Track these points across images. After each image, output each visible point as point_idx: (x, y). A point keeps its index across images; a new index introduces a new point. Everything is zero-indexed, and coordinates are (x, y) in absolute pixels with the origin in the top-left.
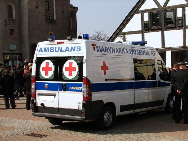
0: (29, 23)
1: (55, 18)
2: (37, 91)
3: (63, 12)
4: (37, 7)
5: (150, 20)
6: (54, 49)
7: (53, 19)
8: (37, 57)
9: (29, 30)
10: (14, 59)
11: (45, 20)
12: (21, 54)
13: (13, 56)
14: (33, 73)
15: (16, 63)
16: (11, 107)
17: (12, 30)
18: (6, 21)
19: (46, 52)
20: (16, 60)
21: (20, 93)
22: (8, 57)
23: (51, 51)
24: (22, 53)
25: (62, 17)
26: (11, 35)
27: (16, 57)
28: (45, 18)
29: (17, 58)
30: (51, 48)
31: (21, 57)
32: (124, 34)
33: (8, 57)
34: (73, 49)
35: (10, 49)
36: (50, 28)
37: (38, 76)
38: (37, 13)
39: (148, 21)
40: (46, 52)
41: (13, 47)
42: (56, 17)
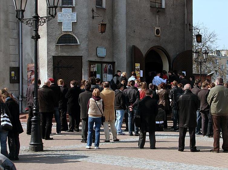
0: (127, 14)
7: (160, 7)
10: (103, 72)
11: (150, 8)
12: (113, 63)
15: (106, 76)
16: (147, 145)
17: (104, 25)
18: (93, 11)
20: (106, 72)
21: (67, 123)
22: (95, 69)
24: (115, 61)
25: (174, 4)
26: (102, 32)
27: (106, 67)
28: (149, 6)
29: (107, 69)
33: (95, 67)
35: (98, 55)
36: (156, 21)
41: (102, 52)
42: (166, 4)
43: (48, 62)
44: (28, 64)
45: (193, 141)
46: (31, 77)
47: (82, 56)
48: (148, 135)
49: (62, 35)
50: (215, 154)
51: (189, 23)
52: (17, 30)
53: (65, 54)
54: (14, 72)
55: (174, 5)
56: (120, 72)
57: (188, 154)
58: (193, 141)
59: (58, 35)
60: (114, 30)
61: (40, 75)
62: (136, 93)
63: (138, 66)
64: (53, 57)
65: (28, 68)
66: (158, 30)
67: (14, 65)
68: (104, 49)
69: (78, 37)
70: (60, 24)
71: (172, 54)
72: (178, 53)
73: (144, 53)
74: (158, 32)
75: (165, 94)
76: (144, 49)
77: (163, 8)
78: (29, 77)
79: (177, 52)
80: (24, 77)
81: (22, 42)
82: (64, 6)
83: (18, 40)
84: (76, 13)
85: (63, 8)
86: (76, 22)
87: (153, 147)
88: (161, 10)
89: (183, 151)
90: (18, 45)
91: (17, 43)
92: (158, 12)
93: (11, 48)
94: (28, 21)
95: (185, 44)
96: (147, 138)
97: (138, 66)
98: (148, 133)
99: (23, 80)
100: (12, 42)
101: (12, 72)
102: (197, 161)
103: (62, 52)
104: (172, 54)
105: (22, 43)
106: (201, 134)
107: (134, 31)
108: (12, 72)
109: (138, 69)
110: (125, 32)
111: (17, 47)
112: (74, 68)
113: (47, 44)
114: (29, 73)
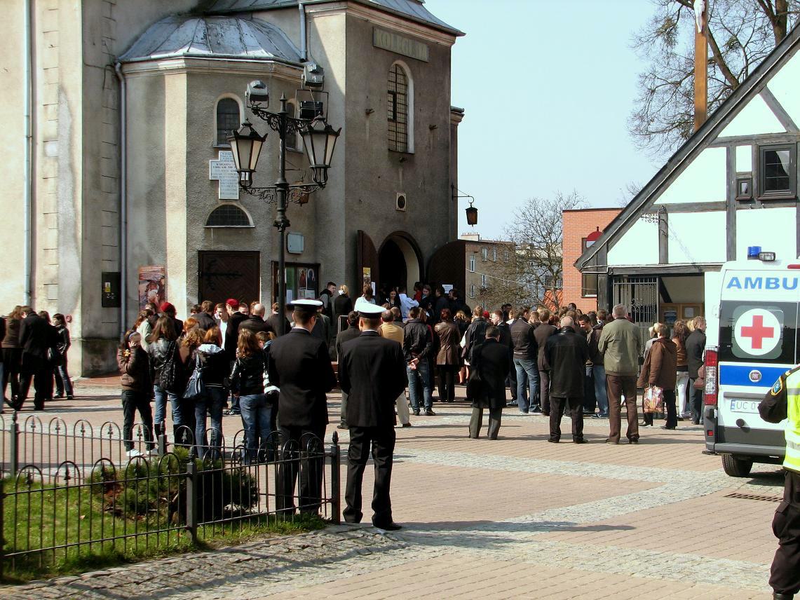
1: (411, 149)
2: (720, 386)
3: (432, 128)
4: (368, 112)
5: (757, 170)
6: (780, 283)
8: (724, 299)
9: (348, 190)
11: (387, 153)
12: (316, 267)
13: (296, 272)
14: (712, 342)
16: (484, 432)
19: (753, 286)
20: (303, 285)
23: (768, 287)
24: (320, 261)
27: (303, 275)
28: (385, 148)
29: (305, 279)
30: (768, 280)
31: (315, 275)
32: (665, 210)
34: (751, 282)
37: (727, 348)
38: (368, 131)
39: (751, 173)
40: (753, 286)
42: (416, 144)
43: (189, 263)
44: (140, 267)
45: (578, 425)
46: (147, 295)
47: (259, 252)
48: (486, 415)
49: (217, 206)
50: (612, 448)
52: (116, 195)
55: (430, 147)
56: (335, 285)
57: (568, 447)
58: (578, 425)
59: (209, 207)
60: (318, 197)
61: (168, 291)
62: (425, 331)
63: (367, 272)
64: (200, 252)
65: (140, 276)
66: (401, 199)
67: (111, 268)
68: (299, 236)
69: (250, 212)
70: (215, 183)
71: (427, 248)
72: (436, 247)
73: (378, 245)
74: (401, 202)
75: (452, 333)
76: (377, 237)
78: (143, 293)
79: (435, 245)
80: (130, 294)
81: (126, 219)
82: (222, 146)
83: (117, 216)
87: (494, 436)
88: (406, 156)
89: (558, 442)
90: (117, 226)
91: (117, 221)
92: (401, 161)
93: (105, 232)
94: (265, 191)
95: (450, 227)
96: (485, 420)
97: (367, 272)
98: (486, 411)
99: (129, 300)
101: (106, 284)
102: (714, 462)
103: (217, 243)
104: (427, 248)
105: (126, 223)
106: (540, 411)
107: (360, 200)
108: (106, 284)
109: (368, 279)
110: (342, 201)
111: (116, 230)
112: (241, 276)
113: (185, 225)
114: (143, 286)
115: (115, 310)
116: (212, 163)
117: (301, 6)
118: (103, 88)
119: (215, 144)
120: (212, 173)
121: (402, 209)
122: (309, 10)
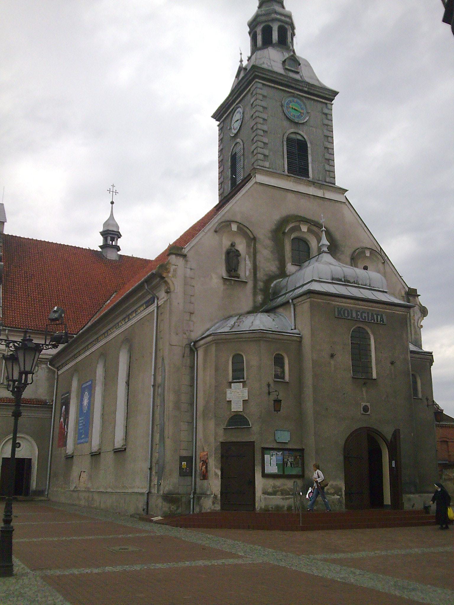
4: (332, 356)
18: (269, 385)
35: (277, 438)
51: (425, 397)
53: (234, 440)
54: (185, 463)
64: (222, 443)
69: (249, 418)
74: (366, 409)
77: (374, 378)
84: (247, 388)
85: (232, 384)
86: (247, 399)
100: (184, 426)
101: (183, 463)
108: (183, 463)
115: (189, 478)
116: (228, 391)
117: (290, 301)
118: (184, 356)
119: (230, 380)
120: (229, 397)
121: (367, 413)
122: (295, 301)
